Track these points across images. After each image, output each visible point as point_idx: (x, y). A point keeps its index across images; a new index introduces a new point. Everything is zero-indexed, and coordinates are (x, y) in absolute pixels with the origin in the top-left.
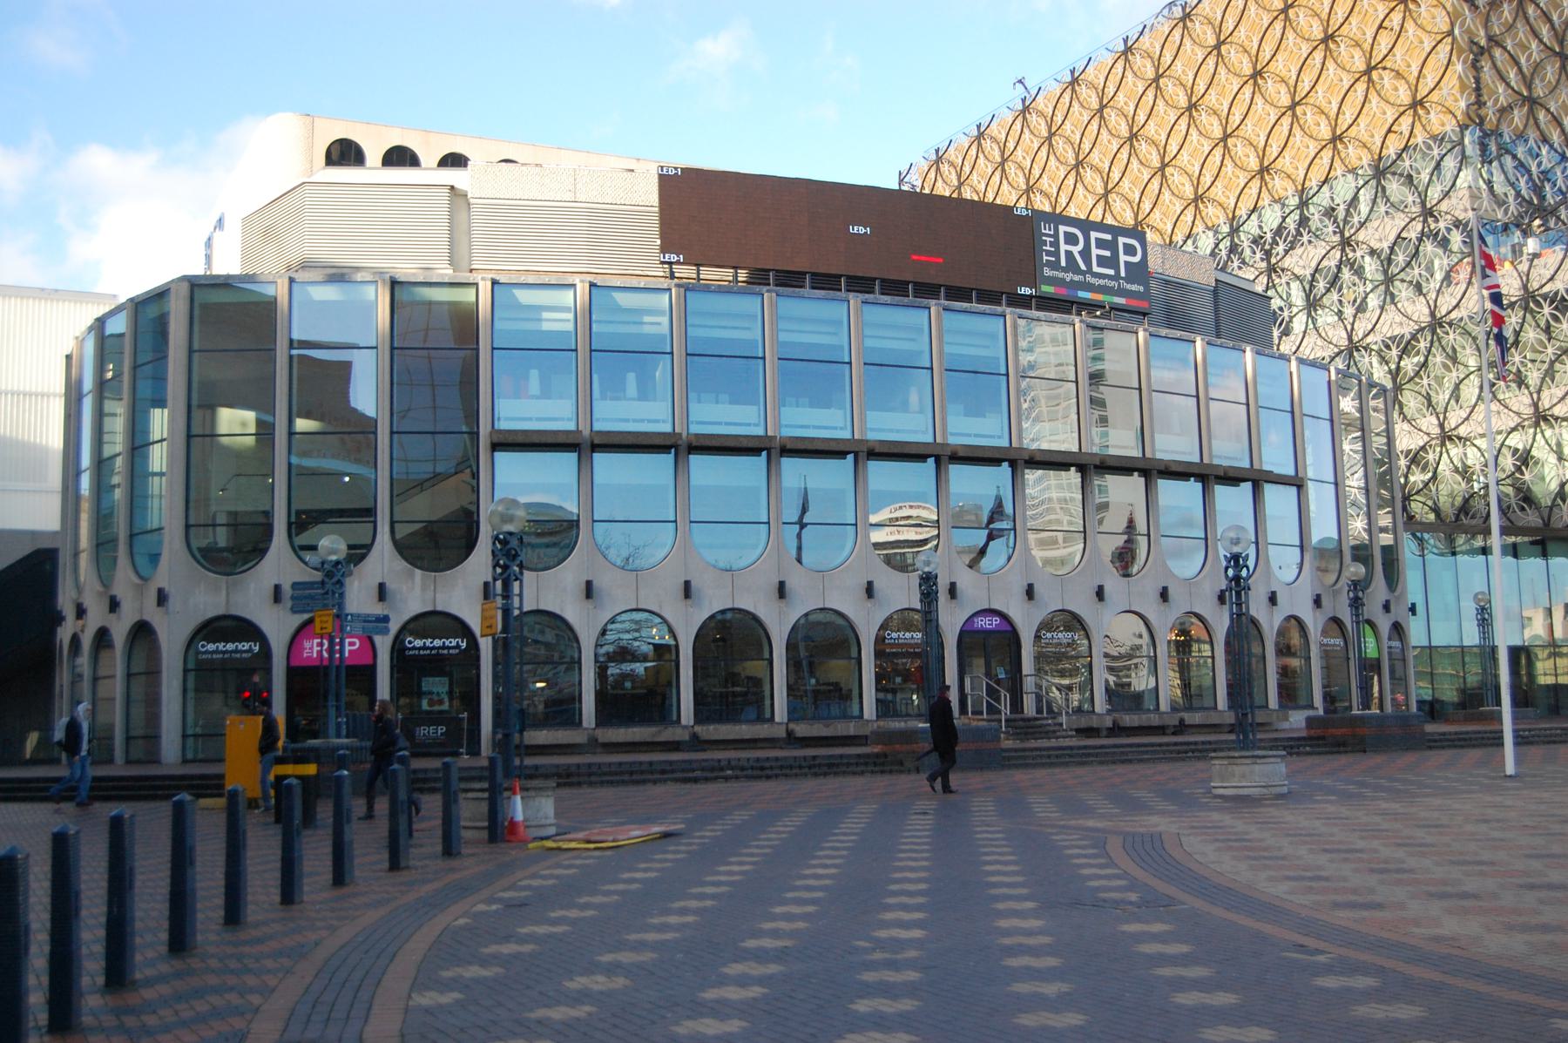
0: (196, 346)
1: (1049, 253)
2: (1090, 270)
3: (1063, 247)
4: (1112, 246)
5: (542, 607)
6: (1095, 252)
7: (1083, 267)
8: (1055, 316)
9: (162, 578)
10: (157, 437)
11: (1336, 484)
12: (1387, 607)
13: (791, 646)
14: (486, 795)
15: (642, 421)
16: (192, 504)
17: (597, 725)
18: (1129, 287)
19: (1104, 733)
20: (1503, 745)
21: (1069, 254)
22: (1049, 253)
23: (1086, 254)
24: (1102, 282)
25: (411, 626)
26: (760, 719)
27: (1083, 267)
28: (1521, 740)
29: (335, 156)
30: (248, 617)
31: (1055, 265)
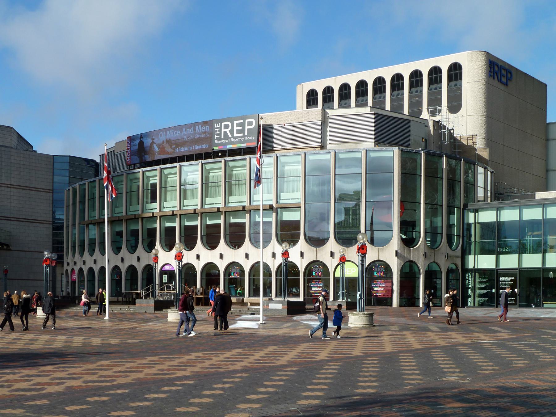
1: (217, 135)
3: (223, 130)
4: (243, 125)
6: (236, 128)
7: (230, 136)
10: (362, 340)
14: (210, 184)
16: (337, 160)
18: (249, 138)
19: (347, 217)
21: (225, 133)
22: (217, 135)
23: (232, 131)
24: (237, 140)
27: (230, 136)
29: (362, 86)
30: (310, 247)
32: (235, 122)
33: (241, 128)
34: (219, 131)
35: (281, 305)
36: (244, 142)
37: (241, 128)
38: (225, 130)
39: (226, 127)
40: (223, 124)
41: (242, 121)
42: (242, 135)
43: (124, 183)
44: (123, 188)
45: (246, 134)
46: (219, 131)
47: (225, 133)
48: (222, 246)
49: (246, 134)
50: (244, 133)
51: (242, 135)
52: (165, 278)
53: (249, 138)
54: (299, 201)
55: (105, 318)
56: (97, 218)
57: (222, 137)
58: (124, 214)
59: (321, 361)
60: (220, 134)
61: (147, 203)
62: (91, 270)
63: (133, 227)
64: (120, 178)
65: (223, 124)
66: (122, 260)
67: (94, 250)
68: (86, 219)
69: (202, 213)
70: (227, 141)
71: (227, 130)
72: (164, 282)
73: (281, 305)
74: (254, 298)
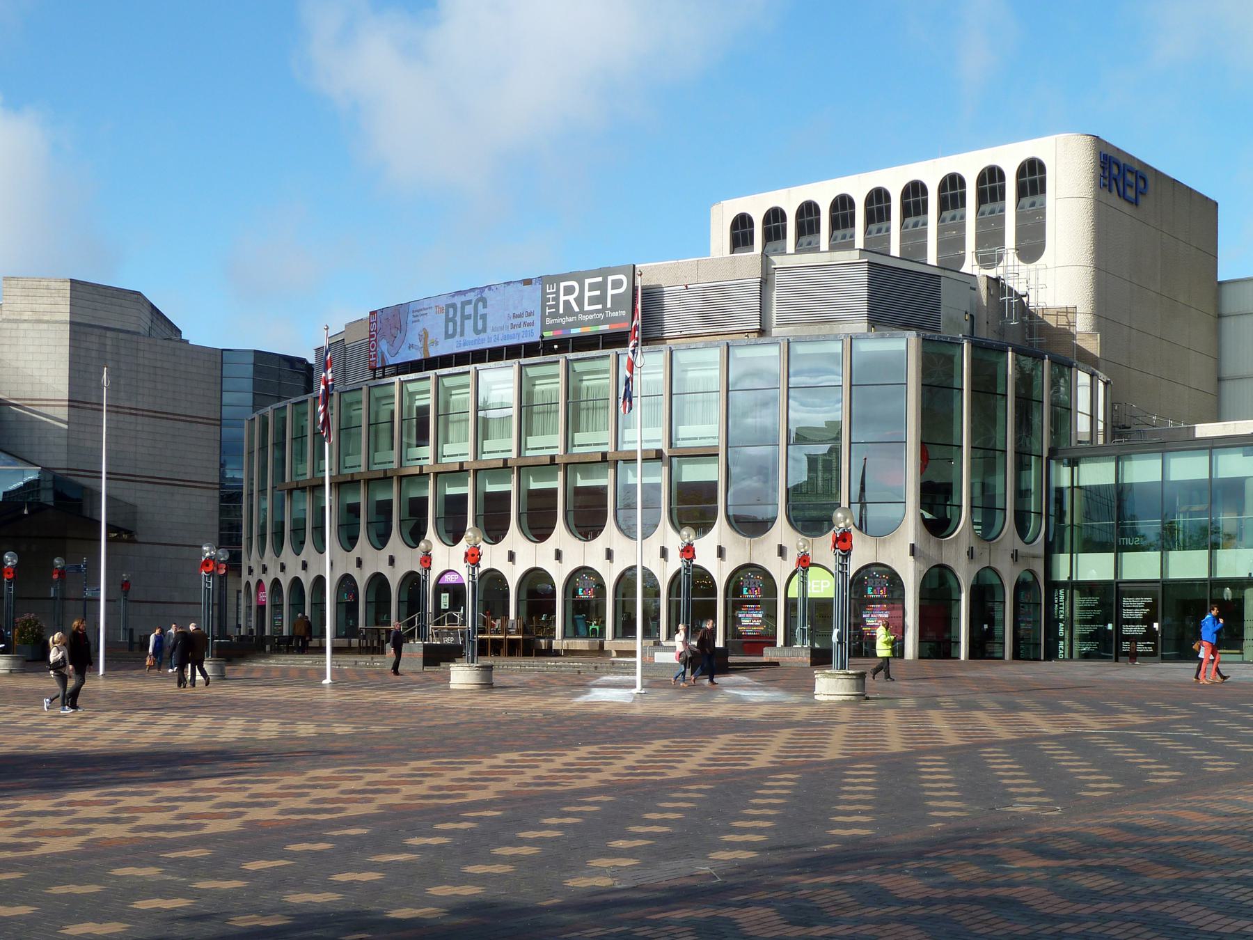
1: (551, 307)
2: (582, 312)
3: (562, 298)
4: (602, 287)
6: (587, 294)
7: (576, 309)
9: (283, 559)
11: (1091, 416)
17: (812, 664)
21: (567, 303)
22: (551, 307)
23: (579, 300)
24: (590, 317)
27: (576, 309)
28: (335, 650)
31: (555, 315)
32: (587, 281)
33: (598, 293)
37: (598, 293)
38: (567, 298)
39: (568, 291)
41: (600, 279)
42: (600, 307)
43: (364, 406)
44: (360, 415)
45: (609, 305)
48: (561, 535)
49: (609, 305)
50: (605, 304)
51: (600, 307)
52: (445, 599)
56: (308, 476)
57: (561, 311)
58: (363, 469)
60: (557, 306)
61: (409, 446)
63: (381, 496)
65: (562, 285)
66: (359, 563)
68: (287, 479)
70: (570, 320)
71: (571, 298)
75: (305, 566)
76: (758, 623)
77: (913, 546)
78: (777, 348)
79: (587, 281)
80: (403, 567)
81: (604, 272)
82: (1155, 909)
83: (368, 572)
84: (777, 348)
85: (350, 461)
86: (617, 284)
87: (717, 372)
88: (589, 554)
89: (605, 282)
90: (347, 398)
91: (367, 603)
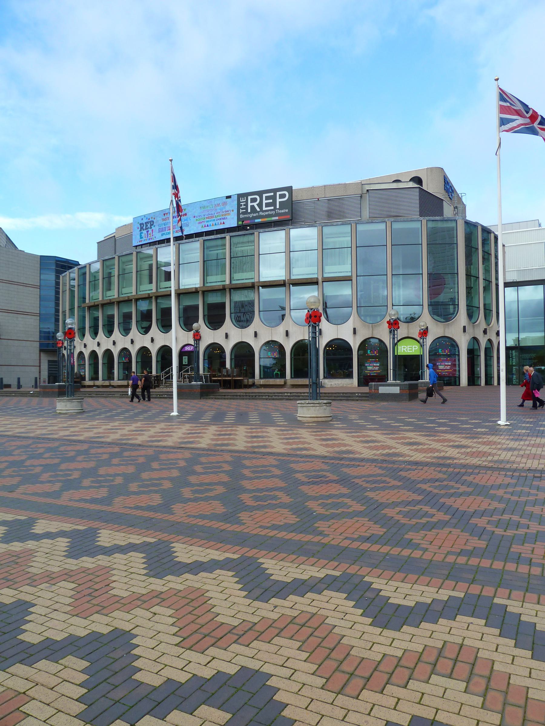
0: (455, 245)
1: (242, 209)
3: (250, 204)
4: (274, 198)
5: (189, 343)
6: (264, 202)
7: (258, 209)
8: (267, 230)
12: (485, 332)
13: (326, 352)
15: (336, 272)
18: (281, 211)
20: (172, 398)
21: (252, 207)
22: (242, 209)
23: (260, 205)
24: (267, 213)
25: (382, 344)
26: (325, 378)
27: (258, 209)
31: (246, 213)
32: (264, 195)
33: (271, 201)
34: (244, 205)
35: (398, 388)
36: (275, 216)
37: (271, 201)
38: (252, 204)
40: (249, 198)
41: (272, 194)
42: (272, 208)
43: (134, 262)
44: (132, 268)
45: (278, 207)
46: (244, 205)
47: (252, 207)
48: (228, 325)
49: (278, 207)
50: (275, 206)
51: (272, 208)
52: (185, 360)
53: (281, 211)
54: (316, 276)
55: (172, 414)
56: (100, 299)
57: (249, 211)
58: (134, 293)
59: (189, 423)
60: (246, 208)
61: (161, 281)
62: (94, 354)
63: (126, 310)
64: (129, 258)
65: (249, 198)
66: (99, 344)
67: (84, 335)
68: (87, 301)
69: (230, 289)
70: (255, 215)
71: (255, 204)
72: (184, 363)
73: (398, 388)
74: (296, 380)
75: (85, 346)
76: (377, 368)
77: (464, 327)
78: (384, 224)
79: (264, 195)
80: (159, 343)
81: (275, 191)
82: (238, 530)
83: (138, 346)
84: (384, 224)
85: (125, 291)
86: (282, 196)
87: (199, 254)
88: (245, 335)
89: (275, 195)
90: (123, 259)
91: (157, 361)
